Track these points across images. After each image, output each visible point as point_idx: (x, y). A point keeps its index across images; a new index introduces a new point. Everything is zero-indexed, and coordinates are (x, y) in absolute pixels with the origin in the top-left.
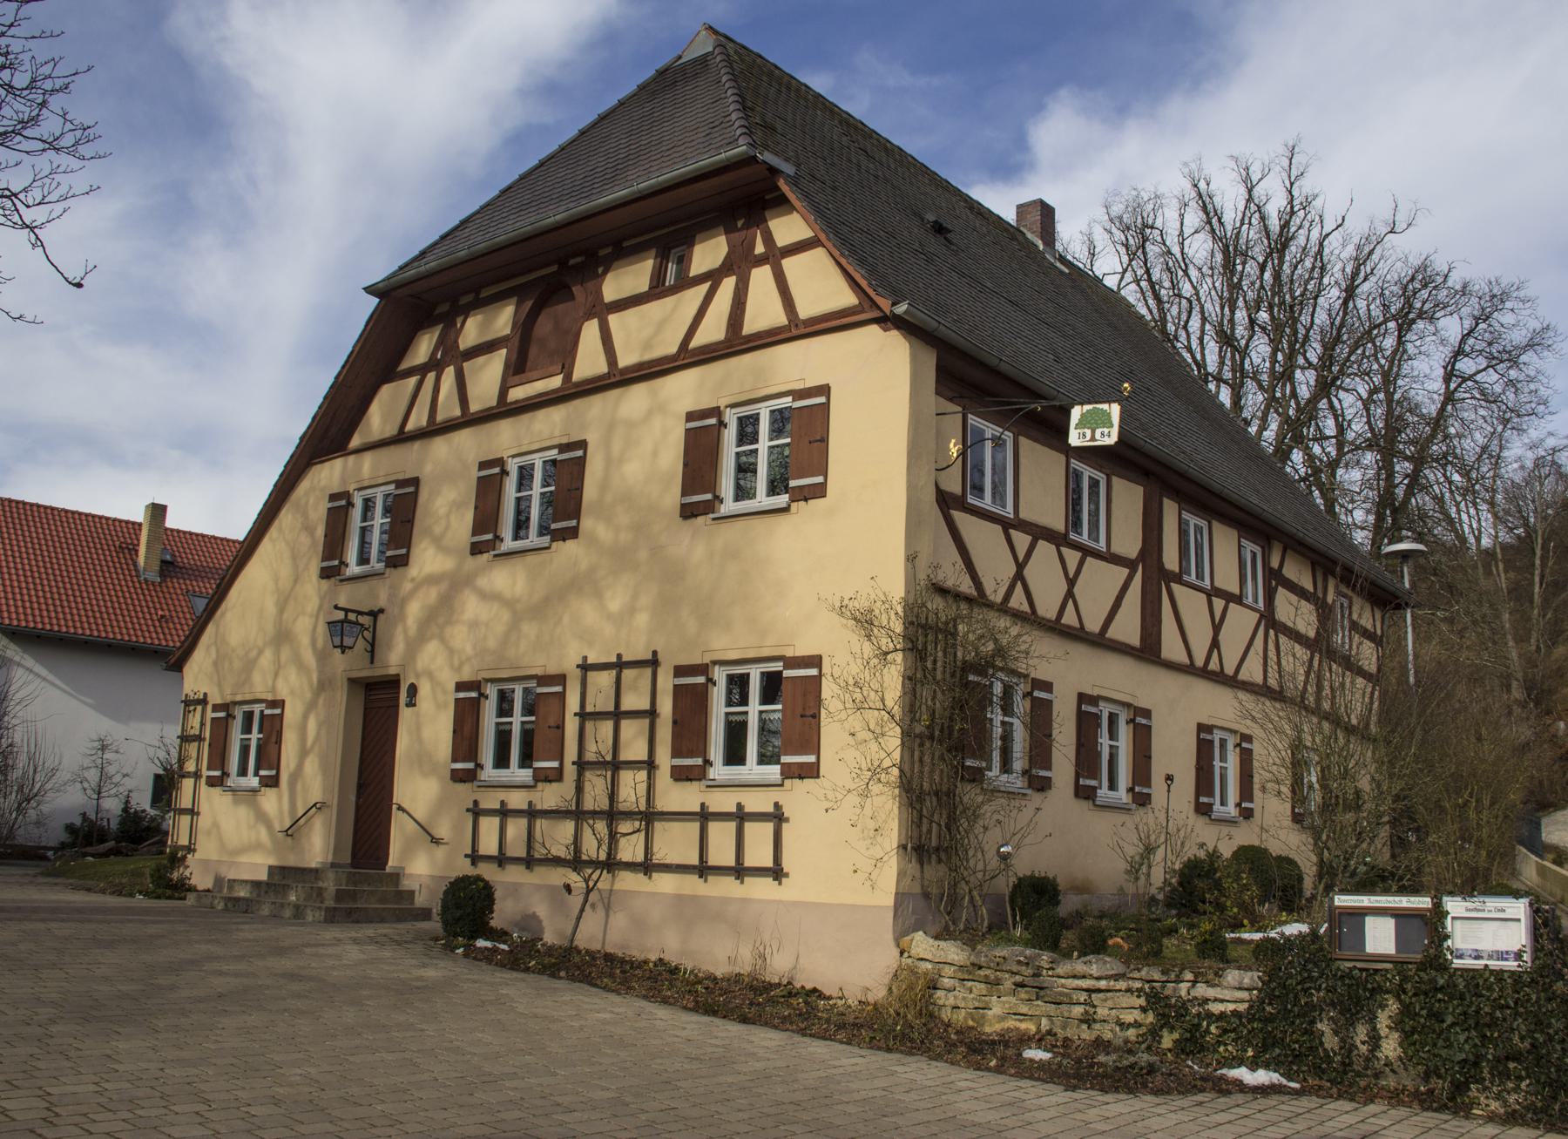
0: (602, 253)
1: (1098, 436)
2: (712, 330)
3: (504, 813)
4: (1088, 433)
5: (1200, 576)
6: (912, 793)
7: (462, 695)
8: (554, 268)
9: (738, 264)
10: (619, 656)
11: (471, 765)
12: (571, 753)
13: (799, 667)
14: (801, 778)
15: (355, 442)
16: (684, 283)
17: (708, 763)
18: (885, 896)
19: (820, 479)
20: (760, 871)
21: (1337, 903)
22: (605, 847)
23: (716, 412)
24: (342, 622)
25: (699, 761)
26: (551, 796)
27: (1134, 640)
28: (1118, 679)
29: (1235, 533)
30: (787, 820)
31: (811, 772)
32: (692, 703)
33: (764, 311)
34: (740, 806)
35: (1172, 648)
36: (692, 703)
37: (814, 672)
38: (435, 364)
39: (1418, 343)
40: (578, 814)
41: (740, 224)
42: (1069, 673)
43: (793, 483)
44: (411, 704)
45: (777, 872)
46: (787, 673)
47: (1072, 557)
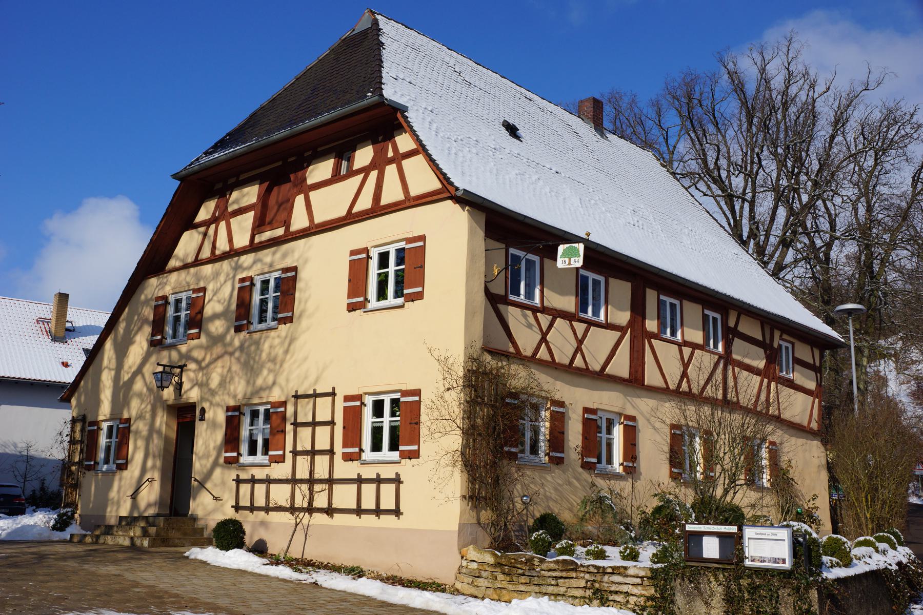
0: (307, 154)
1: (572, 262)
2: (364, 203)
3: (253, 481)
4: (567, 260)
5: (673, 333)
6: (470, 465)
7: (230, 414)
8: (280, 163)
9: (379, 164)
10: (315, 390)
11: (235, 454)
12: (289, 447)
13: (409, 396)
14: (410, 458)
15: (173, 263)
16: (351, 173)
17: (361, 450)
18: (453, 525)
19: (420, 289)
20: (388, 512)
21: (736, 528)
22: (306, 500)
23: (366, 250)
24: (161, 372)
25: (357, 450)
26: (281, 470)
27: (625, 373)
28: (607, 400)
29: (699, 307)
30: (402, 482)
31: (415, 455)
32: (353, 417)
33: (392, 193)
34: (378, 475)
35: (652, 377)
36: (353, 417)
37: (416, 398)
38: (215, 220)
39: (892, 162)
40: (293, 481)
41: (380, 138)
42: (578, 398)
43: (406, 292)
44: (202, 419)
45: (397, 512)
46: (402, 400)
47: (580, 327)
